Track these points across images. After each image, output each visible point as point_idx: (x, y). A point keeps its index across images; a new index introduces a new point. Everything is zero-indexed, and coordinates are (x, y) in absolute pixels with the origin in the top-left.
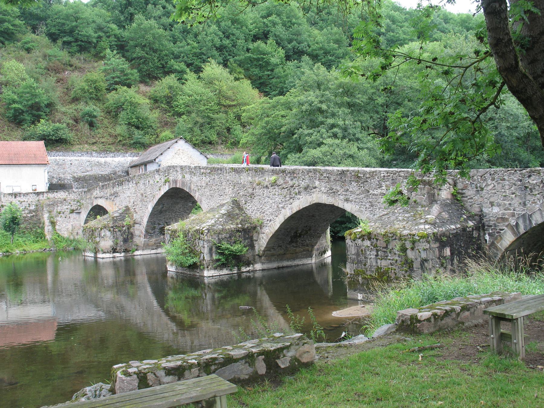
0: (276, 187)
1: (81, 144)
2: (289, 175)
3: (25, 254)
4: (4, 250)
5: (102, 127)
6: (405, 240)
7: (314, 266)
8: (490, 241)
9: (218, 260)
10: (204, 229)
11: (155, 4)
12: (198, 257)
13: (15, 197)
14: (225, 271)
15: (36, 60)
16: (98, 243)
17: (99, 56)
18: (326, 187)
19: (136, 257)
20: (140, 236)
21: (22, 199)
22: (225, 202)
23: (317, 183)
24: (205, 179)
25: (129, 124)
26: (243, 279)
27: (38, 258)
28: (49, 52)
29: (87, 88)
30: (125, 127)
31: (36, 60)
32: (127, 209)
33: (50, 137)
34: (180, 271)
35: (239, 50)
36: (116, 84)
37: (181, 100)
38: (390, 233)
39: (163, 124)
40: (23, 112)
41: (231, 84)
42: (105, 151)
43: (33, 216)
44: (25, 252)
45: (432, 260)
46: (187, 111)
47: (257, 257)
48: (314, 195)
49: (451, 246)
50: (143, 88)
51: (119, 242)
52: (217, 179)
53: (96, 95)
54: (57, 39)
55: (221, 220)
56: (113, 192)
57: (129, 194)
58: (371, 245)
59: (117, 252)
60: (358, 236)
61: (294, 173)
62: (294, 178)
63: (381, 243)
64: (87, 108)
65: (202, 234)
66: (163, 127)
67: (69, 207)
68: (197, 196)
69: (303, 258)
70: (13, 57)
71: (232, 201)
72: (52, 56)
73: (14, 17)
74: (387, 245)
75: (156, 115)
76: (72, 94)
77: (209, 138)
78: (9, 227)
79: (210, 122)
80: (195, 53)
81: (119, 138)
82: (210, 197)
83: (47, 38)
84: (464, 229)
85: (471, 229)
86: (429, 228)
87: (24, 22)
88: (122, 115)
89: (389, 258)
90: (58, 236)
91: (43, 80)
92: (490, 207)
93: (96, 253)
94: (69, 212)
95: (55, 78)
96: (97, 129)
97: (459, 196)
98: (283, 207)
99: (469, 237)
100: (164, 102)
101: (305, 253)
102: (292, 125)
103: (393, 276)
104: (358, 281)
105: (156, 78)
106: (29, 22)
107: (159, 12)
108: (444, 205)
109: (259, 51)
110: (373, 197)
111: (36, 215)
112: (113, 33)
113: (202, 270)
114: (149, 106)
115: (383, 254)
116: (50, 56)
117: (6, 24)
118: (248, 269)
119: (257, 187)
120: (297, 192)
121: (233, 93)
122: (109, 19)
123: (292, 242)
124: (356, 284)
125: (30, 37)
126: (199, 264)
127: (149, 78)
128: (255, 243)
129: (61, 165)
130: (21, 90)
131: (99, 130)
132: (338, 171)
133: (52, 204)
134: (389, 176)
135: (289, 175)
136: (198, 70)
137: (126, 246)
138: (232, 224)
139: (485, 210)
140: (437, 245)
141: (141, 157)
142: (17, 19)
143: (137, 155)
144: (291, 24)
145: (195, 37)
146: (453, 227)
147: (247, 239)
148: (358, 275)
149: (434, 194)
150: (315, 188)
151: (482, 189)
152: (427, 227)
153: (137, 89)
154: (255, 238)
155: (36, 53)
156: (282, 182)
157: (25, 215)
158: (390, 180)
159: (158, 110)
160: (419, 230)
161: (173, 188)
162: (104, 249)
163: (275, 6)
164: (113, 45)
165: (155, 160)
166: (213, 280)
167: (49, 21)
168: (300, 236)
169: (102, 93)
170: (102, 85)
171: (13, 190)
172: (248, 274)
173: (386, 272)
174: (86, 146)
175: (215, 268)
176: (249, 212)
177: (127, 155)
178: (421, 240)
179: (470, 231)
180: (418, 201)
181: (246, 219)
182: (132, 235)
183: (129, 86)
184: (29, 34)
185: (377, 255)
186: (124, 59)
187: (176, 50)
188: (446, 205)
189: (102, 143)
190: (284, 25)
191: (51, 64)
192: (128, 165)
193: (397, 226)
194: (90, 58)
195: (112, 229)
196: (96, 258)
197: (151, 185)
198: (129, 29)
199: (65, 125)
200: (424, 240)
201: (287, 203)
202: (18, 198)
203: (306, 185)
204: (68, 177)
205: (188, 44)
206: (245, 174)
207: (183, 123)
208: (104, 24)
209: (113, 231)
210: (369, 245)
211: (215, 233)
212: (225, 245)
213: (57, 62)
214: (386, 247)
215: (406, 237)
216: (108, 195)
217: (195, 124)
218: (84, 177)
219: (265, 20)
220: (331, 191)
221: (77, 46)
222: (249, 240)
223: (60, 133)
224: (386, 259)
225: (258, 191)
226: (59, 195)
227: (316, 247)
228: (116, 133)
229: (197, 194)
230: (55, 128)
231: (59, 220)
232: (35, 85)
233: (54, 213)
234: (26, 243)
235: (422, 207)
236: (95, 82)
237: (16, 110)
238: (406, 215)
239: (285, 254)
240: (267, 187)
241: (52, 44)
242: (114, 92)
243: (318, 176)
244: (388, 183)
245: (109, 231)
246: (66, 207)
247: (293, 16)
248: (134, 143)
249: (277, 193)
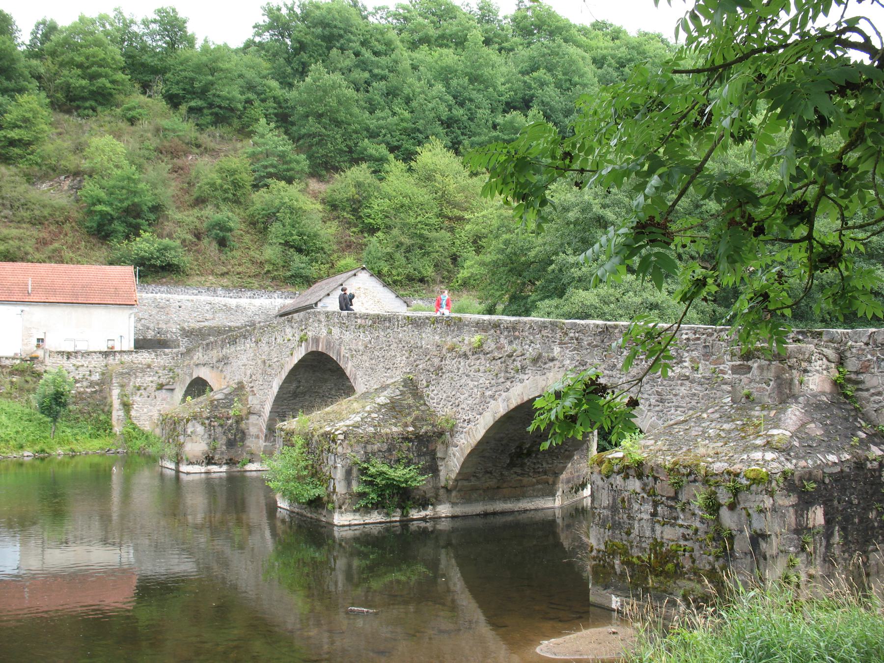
0: (481, 356)
2: (506, 333)
3: (73, 456)
4: (37, 448)
5: (239, 248)
6: (717, 484)
7: (558, 513)
9: (362, 495)
10: (337, 433)
11: (342, 49)
13: (68, 358)
14: (376, 517)
15: (142, 136)
16: (181, 445)
17: (245, 132)
18: (572, 359)
19: (248, 474)
20: (257, 437)
21: (79, 361)
23: (557, 350)
24: (365, 337)
25: (286, 244)
27: (97, 465)
28: (165, 123)
29: (219, 181)
30: (278, 249)
32: (241, 386)
33: (153, 262)
34: (296, 510)
36: (268, 178)
37: (378, 205)
39: (343, 245)
40: (113, 218)
41: (463, 183)
42: (242, 287)
43: (95, 392)
44: (73, 454)
47: (442, 492)
49: (827, 504)
50: (314, 185)
51: (218, 446)
53: (234, 195)
54: (180, 104)
56: (221, 356)
57: (245, 361)
58: (643, 489)
59: (215, 464)
60: (616, 469)
62: (515, 339)
63: (664, 488)
65: (334, 441)
67: (155, 378)
68: (349, 368)
69: (537, 496)
71: (405, 381)
72: (169, 130)
73: (115, 70)
74: (676, 493)
76: (195, 192)
78: (49, 408)
79: (422, 245)
82: (370, 371)
83: (164, 103)
84: (860, 465)
85: (876, 464)
86: (772, 460)
88: (275, 228)
89: (680, 522)
90: (134, 429)
91: (150, 169)
93: (177, 464)
94: (154, 388)
95: (170, 166)
96: (231, 250)
97: (850, 386)
98: (492, 397)
99: (872, 484)
101: (540, 486)
102: (548, 248)
103: (688, 565)
104: (613, 567)
105: (337, 169)
106: (139, 76)
107: (348, 61)
108: (815, 407)
109: (513, 128)
110: (665, 382)
111: (101, 391)
113: (331, 512)
116: (165, 129)
117: (103, 81)
118: (423, 514)
119: (449, 355)
121: (466, 197)
122: (265, 72)
123: (512, 465)
124: (610, 573)
125: (137, 100)
126: (325, 499)
127: (327, 170)
128: (439, 463)
129: (162, 308)
130: (112, 183)
131: (234, 252)
132: (597, 326)
133: (127, 373)
134: (698, 339)
136: (408, 157)
137: (232, 454)
140: (793, 499)
141: (298, 300)
142: (120, 72)
143: (292, 295)
144: (571, 84)
145: (407, 104)
146: (833, 458)
147: (425, 454)
148: (613, 553)
149: (792, 380)
150: (553, 360)
152: (769, 456)
153: (302, 186)
154: (439, 455)
155: (144, 125)
156: (493, 346)
157: (82, 390)
158: (700, 348)
160: (750, 461)
162: (190, 456)
163: (544, 55)
164: (270, 114)
165: (316, 304)
166: (348, 534)
167: (168, 75)
168: (529, 454)
169: (244, 191)
170: (245, 179)
171: (76, 346)
172: (423, 524)
173: (672, 555)
174: (211, 278)
175: (356, 511)
176: (432, 403)
179: (874, 470)
180: (755, 395)
181: (427, 416)
183: (290, 181)
184: (135, 95)
185: (654, 514)
186: (286, 137)
187: (373, 123)
189: (238, 274)
190: (558, 85)
191: (167, 144)
193: (702, 451)
195: (207, 422)
196: (178, 471)
197: (279, 345)
198: (298, 87)
199: (178, 242)
200: (761, 487)
202: (73, 361)
203: (534, 354)
205: (394, 114)
206: (429, 330)
208: (258, 79)
209: (210, 425)
210: (638, 490)
211: (358, 442)
212: (378, 466)
213: (176, 139)
214: (675, 498)
215: (719, 478)
216: (215, 360)
217: (398, 247)
218: (200, 329)
219: (527, 78)
220: (582, 368)
221: (211, 114)
222: (428, 458)
223: (170, 255)
224: (673, 525)
225: (450, 364)
226: (140, 358)
227: (564, 476)
228: (262, 259)
229: (350, 364)
230: (161, 247)
231: (138, 401)
232: (136, 177)
233: (130, 389)
234: (78, 438)
235: (763, 408)
236: (233, 172)
237: (103, 214)
238: (726, 426)
239: (498, 488)
240: (465, 355)
241: (171, 112)
242: (265, 189)
243: (558, 336)
244: (695, 354)
245: (203, 424)
246: (151, 379)
247: (574, 71)
248: (292, 276)
249: (482, 368)
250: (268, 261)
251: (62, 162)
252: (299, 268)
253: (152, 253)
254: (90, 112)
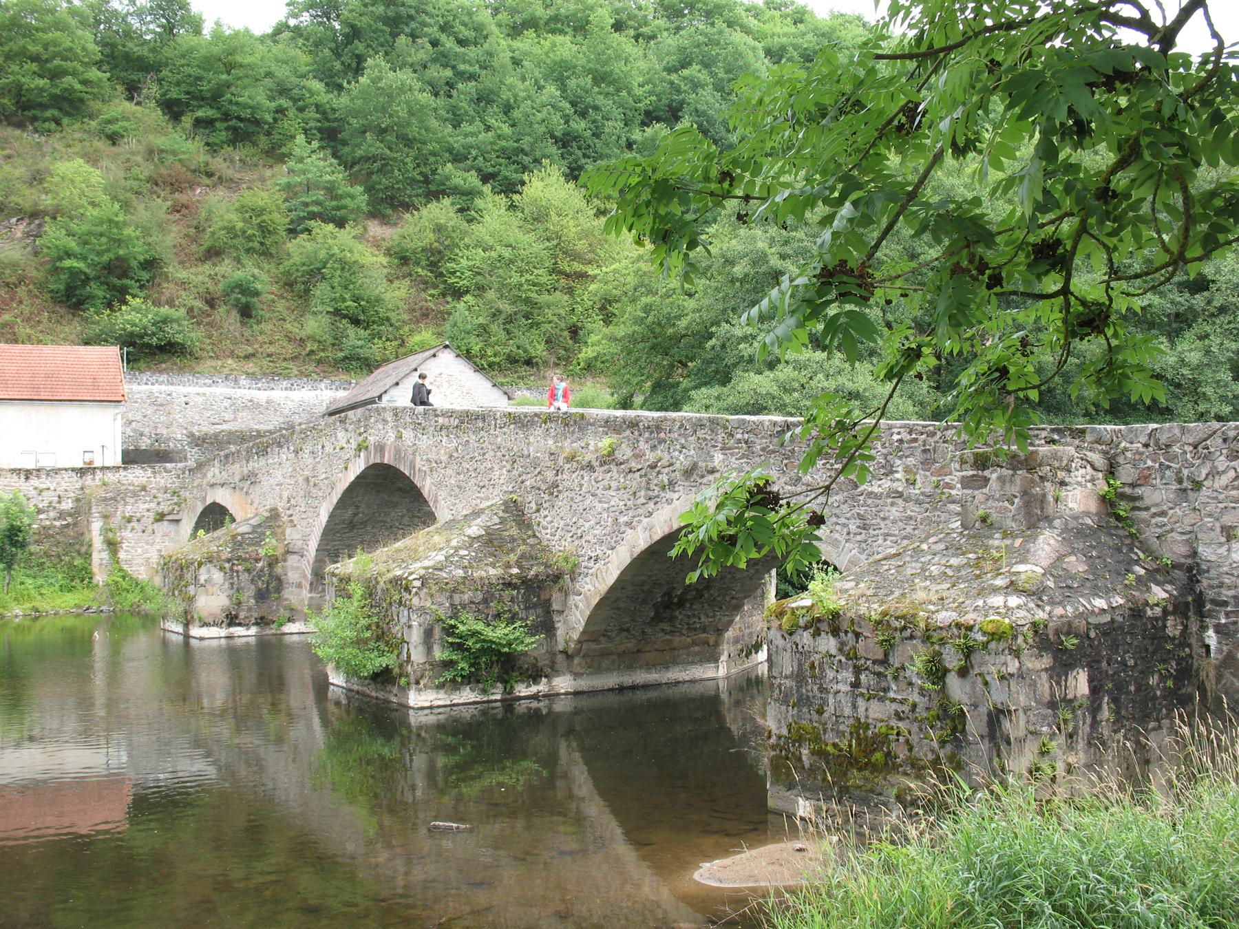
0: (613, 467)
1: (217, 358)
2: (647, 435)
3: (37, 618)
5: (270, 318)
6: (943, 642)
8: (1219, 651)
11: (414, 36)
12: (396, 652)
13: (27, 478)
14: (467, 695)
16: (191, 600)
17: (276, 154)
19: (287, 638)
21: (43, 483)
22: (485, 504)
23: (718, 457)
24: (449, 443)
25: (337, 312)
26: (519, 717)
28: (160, 141)
29: (240, 225)
30: (326, 320)
31: (128, 160)
32: (274, 515)
33: (146, 339)
34: (356, 687)
35: (607, 145)
36: (311, 219)
37: (465, 262)
38: (897, 618)
40: (88, 279)
42: (274, 375)
43: (68, 526)
44: (37, 615)
45: (1026, 710)
46: (476, 284)
47: (560, 658)
50: (375, 229)
51: (243, 599)
52: (473, 444)
53: (262, 244)
54: (182, 113)
55: (463, 552)
56: (246, 472)
57: (280, 479)
58: (840, 650)
59: (240, 625)
60: (802, 622)
61: (659, 428)
62: (660, 443)
63: (869, 647)
65: (407, 589)
67: (153, 505)
68: (427, 486)
69: (693, 663)
70: (76, 154)
71: (505, 503)
72: (166, 152)
74: (886, 655)
79: (529, 312)
80: (504, 150)
81: (310, 346)
82: (456, 489)
83: (160, 112)
85: (1158, 610)
86: (1019, 607)
87: (108, 75)
88: (321, 290)
89: (892, 695)
90: (124, 577)
92: (1221, 545)
94: (151, 520)
95: (169, 203)
96: (259, 322)
98: (629, 524)
101: (697, 649)
103: (902, 754)
104: (800, 759)
105: (407, 207)
106: (123, 74)
107: (423, 52)
108: (1076, 534)
110: (869, 501)
111: (75, 525)
112: (311, 100)
113: (405, 689)
114: (386, 271)
115: (873, 681)
116: (162, 151)
117: (68, 81)
118: (534, 689)
119: (568, 466)
120: (666, 482)
122: (304, 69)
123: (657, 619)
125: (120, 109)
126: (396, 671)
127: (393, 207)
128: (556, 618)
129: (161, 405)
130: (85, 228)
131: (263, 326)
132: (775, 424)
133: (111, 499)
134: (915, 440)
135: (647, 435)
136: (510, 188)
138: (493, 565)
139: (1206, 552)
140: (1046, 661)
141: (355, 392)
143: (346, 385)
146: (1100, 603)
147: (535, 606)
148: (800, 740)
149: (1044, 496)
150: (713, 471)
151: (1197, 485)
152: (1014, 601)
153: (358, 230)
154: (555, 607)
155: (130, 144)
156: (629, 453)
157: (48, 523)
158: (918, 452)
159: (407, 282)
160: (987, 610)
161: (375, 466)
162: (204, 614)
164: (311, 129)
165: (380, 397)
166: (431, 719)
167: (165, 72)
168: (681, 604)
169: (276, 238)
172: (534, 704)
173: (881, 741)
174: (230, 361)
175: (440, 687)
176: (544, 535)
177: (323, 385)
178: (993, 645)
179: (1156, 619)
180: (994, 517)
181: (538, 552)
182: (279, 583)
183: (341, 224)
184: (117, 101)
185: (856, 685)
186: (335, 161)
187: (458, 142)
188: (1081, 533)
189: (269, 356)
190: (719, 87)
191: (164, 172)
192: (323, 409)
193: (920, 596)
195: (227, 565)
196: (187, 636)
197: (328, 455)
199: (183, 311)
200: (1002, 645)
201: (640, 511)
202: (34, 481)
203: (687, 463)
204: (177, 436)
205: (488, 128)
206: (539, 431)
208: (294, 79)
209: (231, 569)
210: (833, 651)
211: (441, 590)
212: (469, 623)
214: (884, 662)
215: (944, 634)
216: (237, 478)
218: (216, 435)
219: (674, 77)
221: (227, 129)
222: (539, 611)
224: (881, 699)
225: (569, 479)
226: (131, 477)
227: (730, 634)
228: (303, 334)
229: (428, 481)
230: (158, 319)
232: (120, 218)
233: (116, 520)
234: (43, 591)
235: (1005, 536)
237: (74, 273)
238: (954, 561)
239: (639, 651)
240: (590, 467)
241: (170, 126)
242: (305, 236)
243: (720, 439)
244: (911, 461)
245: (222, 569)
246: (147, 506)
247: (741, 67)
248: (346, 358)
249: (614, 484)
250: (311, 338)
251: (13, 198)
252: (354, 347)
253: (145, 328)
254: (53, 126)
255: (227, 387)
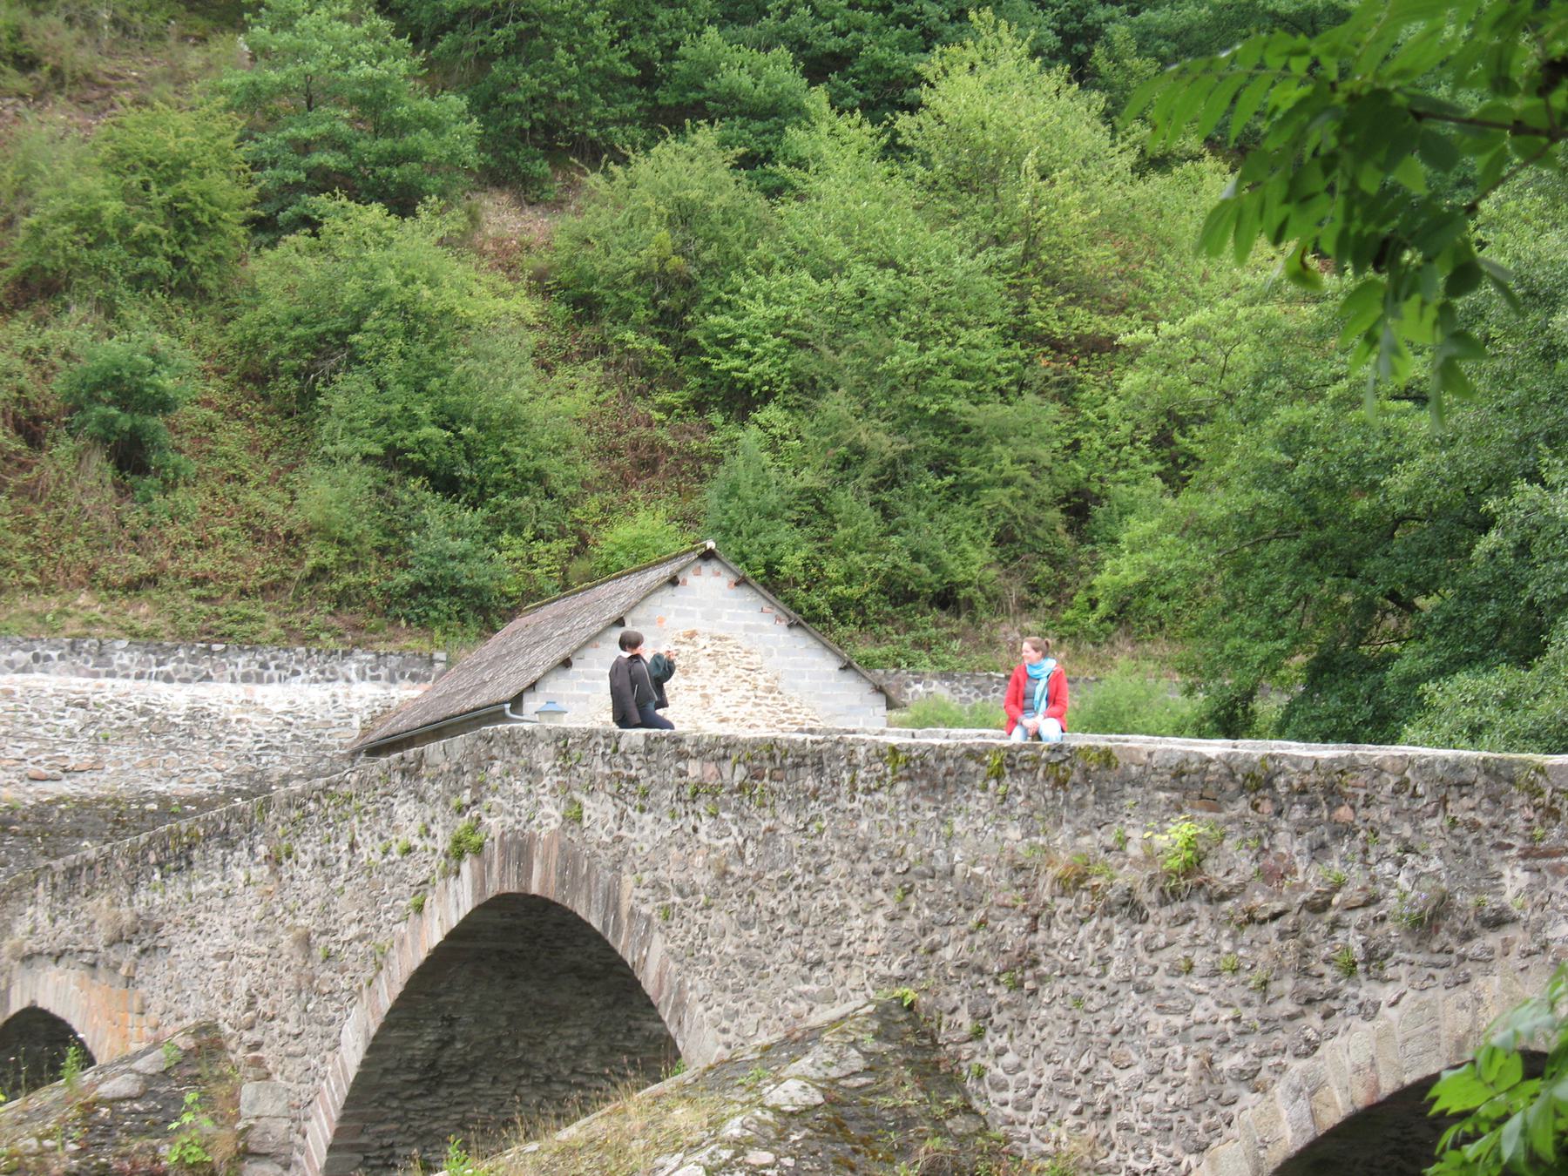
1: (48, 588)
2: (1298, 812)
22: (823, 1015)
25: (393, 458)
30: (360, 479)
36: (317, 191)
39: (625, 461)
48: (1490, 985)
52: (789, 839)
53: (177, 261)
56: (127, 918)
57: (226, 938)
61: (1333, 793)
62: (1337, 835)
64: (114, 349)
66: (625, 483)
71: (883, 1012)
75: (580, 401)
77: (936, 567)
81: (315, 554)
82: (740, 973)
96: (168, 487)
98: (1247, 1077)
100: (641, 314)
105: (595, 153)
114: (532, 339)
119: (1065, 903)
120: (1358, 951)
121: (1124, 257)
127: (553, 154)
131: (180, 495)
135: (1298, 812)
141: (444, 686)
150: (1498, 921)
153: (455, 221)
156: (1245, 866)
159: (592, 371)
165: (517, 702)
170: (222, 196)
174: (84, 599)
176: (997, 1105)
183: (403, 203)
186: (384, 24)
189: (198, 582)
194: (157, 18)
197: (368, 869)
201: (1280, 1038)
206: (980, 802)
207: (766, 457)
216: (101, 937)
217: (845, 464)
218: (41, 811)
228: (295, 519)
236: (171, 170)
242: (301, 239)
248: (418, 587)
249: (1202, 959)
252: (443, 558)
255: (77, 672)
